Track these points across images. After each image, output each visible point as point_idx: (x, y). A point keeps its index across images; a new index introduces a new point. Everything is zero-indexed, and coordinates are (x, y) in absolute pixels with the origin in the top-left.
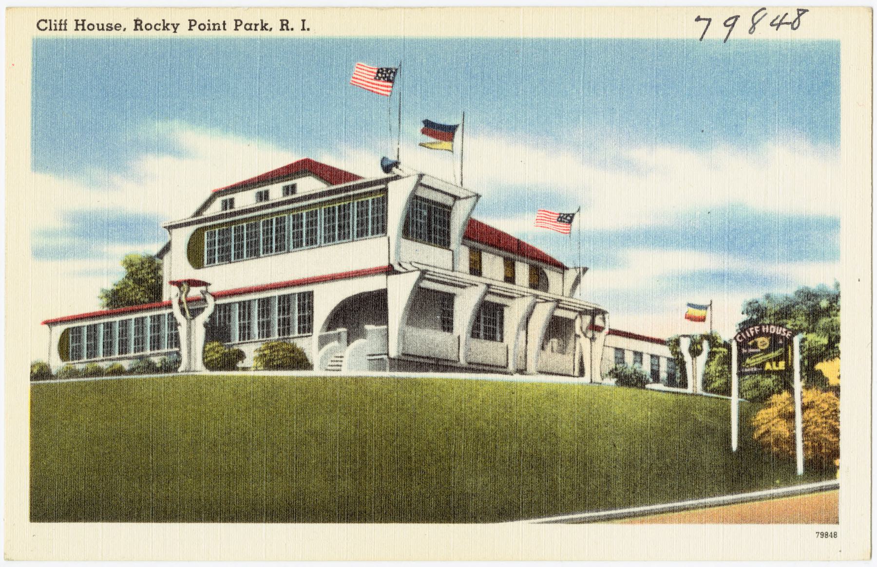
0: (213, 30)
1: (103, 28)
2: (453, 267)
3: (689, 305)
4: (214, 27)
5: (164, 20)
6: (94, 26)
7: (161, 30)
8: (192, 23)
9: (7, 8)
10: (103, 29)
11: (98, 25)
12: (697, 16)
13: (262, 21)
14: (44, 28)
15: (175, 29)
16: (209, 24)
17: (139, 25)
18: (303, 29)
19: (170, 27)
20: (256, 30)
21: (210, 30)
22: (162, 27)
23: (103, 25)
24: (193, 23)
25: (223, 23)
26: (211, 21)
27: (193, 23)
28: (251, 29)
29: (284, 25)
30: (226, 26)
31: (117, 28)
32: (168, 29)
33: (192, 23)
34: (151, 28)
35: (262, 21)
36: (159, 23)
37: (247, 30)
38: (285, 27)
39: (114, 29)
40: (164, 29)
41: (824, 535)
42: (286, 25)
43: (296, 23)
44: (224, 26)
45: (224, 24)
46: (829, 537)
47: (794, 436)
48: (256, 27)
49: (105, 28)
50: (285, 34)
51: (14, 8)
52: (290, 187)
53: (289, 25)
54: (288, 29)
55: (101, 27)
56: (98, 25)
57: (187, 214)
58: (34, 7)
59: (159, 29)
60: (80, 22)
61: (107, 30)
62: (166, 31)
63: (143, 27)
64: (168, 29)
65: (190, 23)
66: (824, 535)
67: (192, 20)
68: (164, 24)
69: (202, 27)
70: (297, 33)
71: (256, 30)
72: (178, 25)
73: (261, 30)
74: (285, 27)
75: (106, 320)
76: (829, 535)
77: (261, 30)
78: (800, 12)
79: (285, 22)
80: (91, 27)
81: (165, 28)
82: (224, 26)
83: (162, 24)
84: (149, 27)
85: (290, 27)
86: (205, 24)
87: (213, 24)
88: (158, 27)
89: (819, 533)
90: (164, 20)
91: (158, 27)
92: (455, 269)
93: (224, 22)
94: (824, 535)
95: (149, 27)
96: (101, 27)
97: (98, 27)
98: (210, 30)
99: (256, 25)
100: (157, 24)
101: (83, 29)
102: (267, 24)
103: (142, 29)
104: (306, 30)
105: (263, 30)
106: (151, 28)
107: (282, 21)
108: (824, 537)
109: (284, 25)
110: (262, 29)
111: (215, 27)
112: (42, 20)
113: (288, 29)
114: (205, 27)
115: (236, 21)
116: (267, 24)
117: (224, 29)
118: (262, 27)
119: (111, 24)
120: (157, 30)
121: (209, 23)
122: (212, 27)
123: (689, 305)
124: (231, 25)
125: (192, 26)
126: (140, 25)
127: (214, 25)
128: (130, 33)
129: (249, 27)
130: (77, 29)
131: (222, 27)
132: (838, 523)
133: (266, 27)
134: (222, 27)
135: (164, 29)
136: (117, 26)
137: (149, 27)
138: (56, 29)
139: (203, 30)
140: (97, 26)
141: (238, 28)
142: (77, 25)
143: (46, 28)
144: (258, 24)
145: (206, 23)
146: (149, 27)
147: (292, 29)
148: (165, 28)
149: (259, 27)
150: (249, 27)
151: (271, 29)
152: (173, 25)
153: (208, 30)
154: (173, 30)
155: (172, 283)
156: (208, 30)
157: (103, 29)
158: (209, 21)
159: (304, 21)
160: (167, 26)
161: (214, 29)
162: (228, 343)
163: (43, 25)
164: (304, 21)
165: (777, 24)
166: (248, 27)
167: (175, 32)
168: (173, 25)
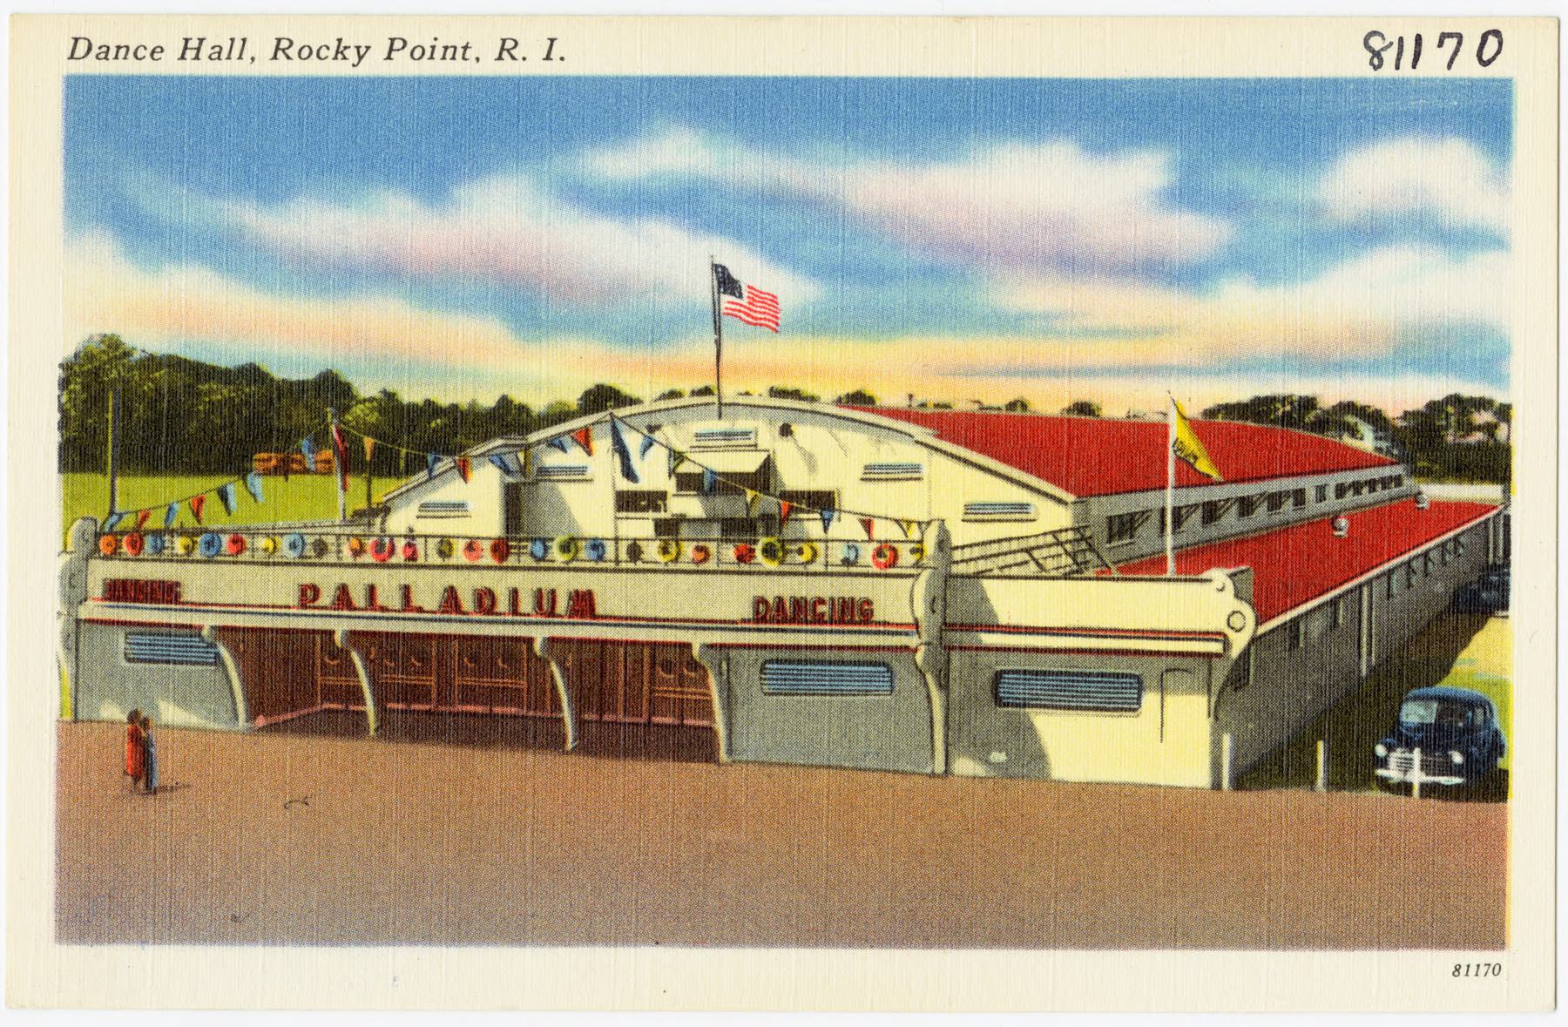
5: (340, 40)
15: (360, 58)
18: (548, 58)
22: (332, 53)
24: (398, 44)
29: (506, 49)
32: (345, 58)
34: (319, 51)
51: (969, 17)
52: (1487, 492)
60: (194, 43)
68: (339, 47)
75: (601, 565)
84: (305, 53)
90: (340, 40)
106: (319, 51)
117: (464, 58)
120: (141, 59)
121: (434, 43)
130: (183, 57)
140: (456, 56)
142: (186, 48)
148: (340, 52)
159: (552, 41)
164: (552, 41)
165: (217, 54)
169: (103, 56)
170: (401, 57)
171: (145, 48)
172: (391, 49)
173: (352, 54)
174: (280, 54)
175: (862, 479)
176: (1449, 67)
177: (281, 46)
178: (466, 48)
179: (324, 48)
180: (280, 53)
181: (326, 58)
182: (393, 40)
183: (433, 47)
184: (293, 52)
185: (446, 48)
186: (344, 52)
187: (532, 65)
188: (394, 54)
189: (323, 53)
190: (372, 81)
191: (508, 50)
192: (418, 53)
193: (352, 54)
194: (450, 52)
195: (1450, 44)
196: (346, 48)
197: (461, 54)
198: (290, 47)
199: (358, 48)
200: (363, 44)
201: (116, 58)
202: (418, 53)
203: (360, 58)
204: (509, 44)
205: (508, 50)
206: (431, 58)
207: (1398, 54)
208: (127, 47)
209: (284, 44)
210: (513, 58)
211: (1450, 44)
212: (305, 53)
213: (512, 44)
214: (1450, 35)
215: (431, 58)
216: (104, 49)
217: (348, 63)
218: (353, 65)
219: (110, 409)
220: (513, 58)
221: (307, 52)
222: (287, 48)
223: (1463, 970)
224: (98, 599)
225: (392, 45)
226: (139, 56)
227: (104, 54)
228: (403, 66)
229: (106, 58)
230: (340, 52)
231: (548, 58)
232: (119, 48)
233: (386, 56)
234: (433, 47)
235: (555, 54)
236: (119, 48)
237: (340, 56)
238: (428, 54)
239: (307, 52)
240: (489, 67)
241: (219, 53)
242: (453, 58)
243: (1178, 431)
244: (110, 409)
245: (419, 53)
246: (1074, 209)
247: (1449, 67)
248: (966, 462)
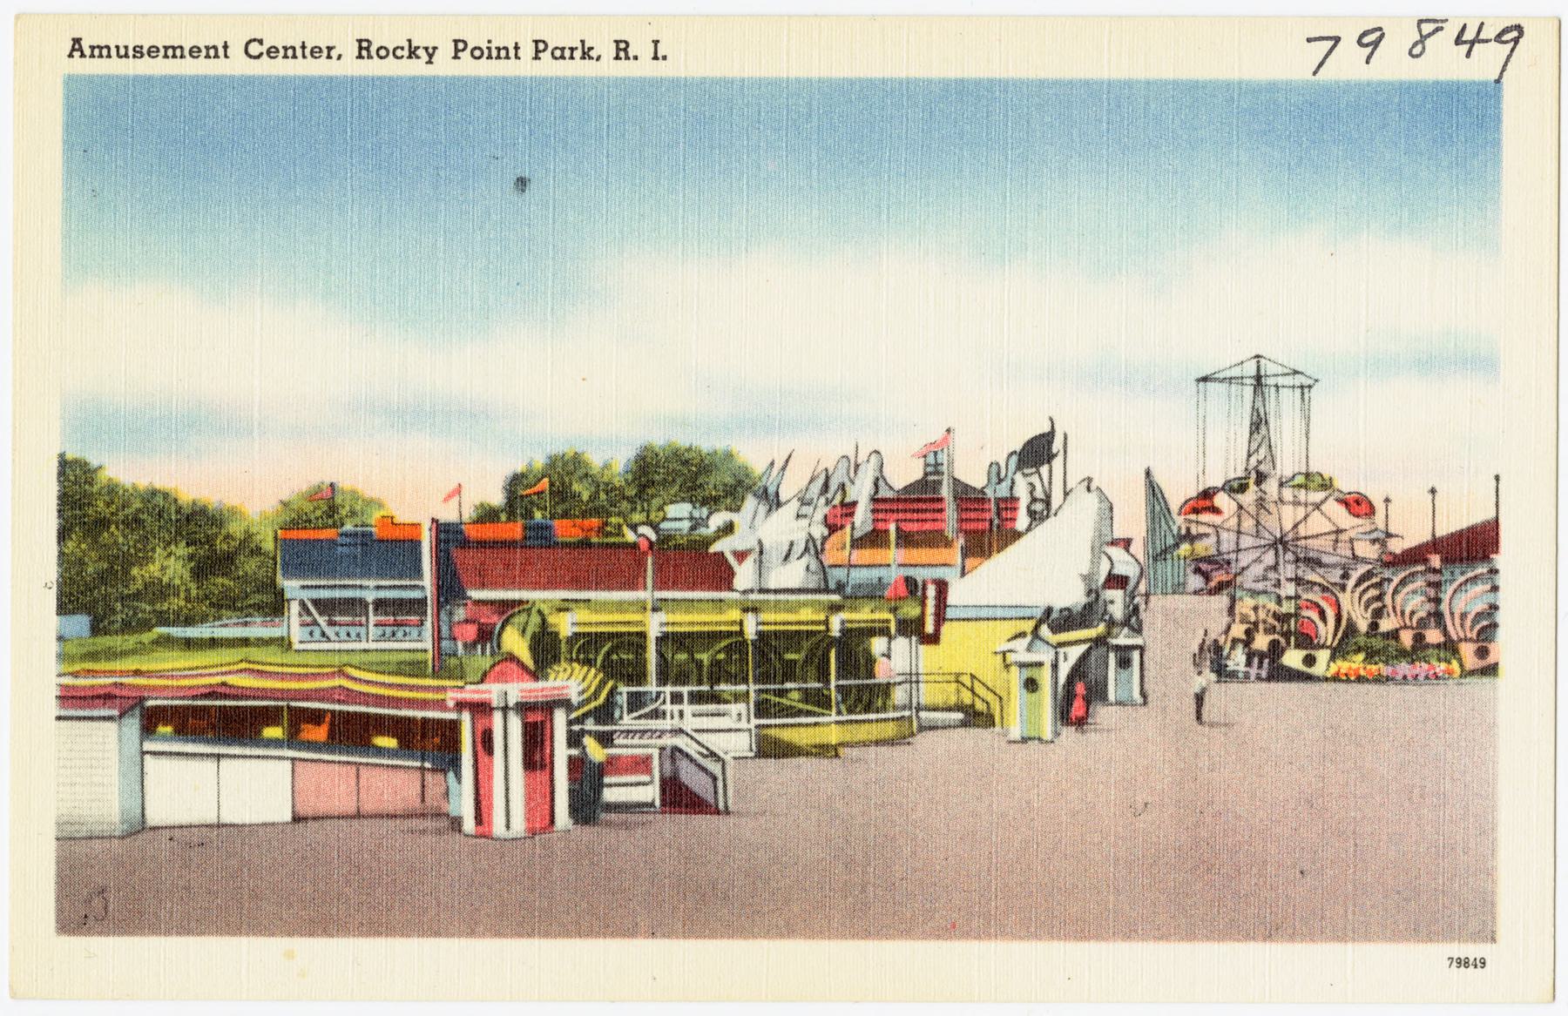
0: (98, 57)
1: (174, 51)
4: (92, 52)
5: (410, 41)
6: (378, 54)
7: (405, 58)
8: (459, 46)
9: (17, 17)
10: (126, 56)
11: (117, 47)
12: (79, 37)
13: (583, 42)
14: (257, 54)
15: (431, 56)
16: (489, 49)
17: (365, 48)
18: (656, 58)
19: (421, 52)
20: (572, 58)
21: (492, 58)
22: (406, 53)
23: (126, 47)
24: (461, 46)
25: (514, 45)
26: (493, 41)
27: (461, 46)
28: (562, 57)
29: (622, 49)
30: (228, 50)
31: (315, 55)
32: (418, 57)
33: (459, 46)
34: (388, 55)
35: (583, 42)
36: (401, 45)
37: (556, 58)
38: (622, 54)
39: (146, 56)
40: (410, 57)
41: (1463, 963)
42: (625, 50)
43: (642, 47)
44: (226, 51)
45: (517, 48)
46: (1472, 967)
47: (377, 610)
48: (572, 54)
49: (131, 53)
50: (624, 69)
53: (629, 50)
54: (627, 58)
55: (122, 52)
56: (117, 47)
57: (1346, 490)
58: (758, 16)
59: (402, 57)
61: (134, 56)
62: (414, 60)
63: (373, 52)
64: (418, 57)
65: (456, 46)
66: (1463, 962)
67: (540, 41)
68: (410, 46)
69: (477, 53)
70: (644, 68)
71: (572, 58)
72: (435, 48)
73: (581, 58)
74: (622, 54)
76: (1470, 963)
77: (581, 58)
78: (1427, 28)
79: (365, 44)
80: (383, 53)
81: (586, 56)
82: (226, 51)
83: (407, 48)
85: (631, 55)
86: (481, 46)
87: (496, 48)
88: (399, 53)
89: (1452, 959)
90: (410, 41)
91: (399, 53)
93: (516, 44)
94: (1463, 963)
95: (383, 53)
96: (122, 52)
97: (182, 51)
98: (492, 58)
99: (572, 49)
100: (398, 48)
101: (370, 57)
102: (592, 48)
103: (370, 57)
104: (632, 58)
105: (585, 58)
107: (360, 41)
108: (1463, 967)
109: (622, 49)
110: (583, 58)
111: (502, 53)
112: (255, 40)
113: (627, 58)
114: (483, 53)
115: (456, 42)
116: (592, 48)
117: (226, 56)
118: (584, 53)
119: (141, 47)
122: (494, 53)
124: (527, 50)
125: (540, 51)
126: (368, 49)
127: (499, 49)
128: (350, 66)
129: (560, 54)
131: (221, 52)
132: (1494, 940)
134: (221, 52)
135: (410, 57)
136: (152, 49)
137: (383, 53)
138: (490, 57)
139: (479, 58)
141: (541, 55)
143: (261, 54)
144: (576, 48)
145: (484, 46)
146: (383, 53)
147: (636, 58)
148: (413, 53)
149: (577, 54)
150: (560, 54)
151: (598, 59)
152: (426, 49)
153: (487, 58)
154: (427, 59)
156: (487, 58)
157: (126, 56)
158: (489, 42)
159: (656, 42)
160: (415, 51)
161: (498, 57)
162: (868, 682)
163: (255, 49)
164: (656, 42)
166: (558, 53)
167: (430, 62)
168: (426, 49)
172: (537, 51)
175: (59, 718)
176: (1315, 73)
178: (330, 49)
181: (402, 57)
190: (1347, 87)
197: (223, 53)
200: (431, 45)
219: (750, 648)
228: (467, 67)
244: (750, 648)
246: (1379, 360)
247: (1315, 73)
248: (91, 719)
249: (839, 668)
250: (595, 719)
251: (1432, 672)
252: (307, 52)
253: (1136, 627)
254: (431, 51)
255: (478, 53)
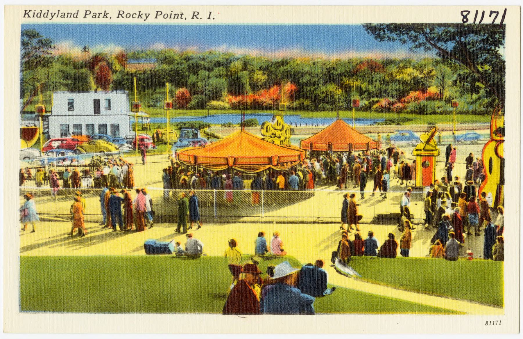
2: (451, 130)
3: (484, 12)
5: (140, 12)
7: (136, 18)
15: (147, 18)
18: (209, 18)
22: (137, 16)
24: (159, 13)
29: (195, 15)
32: (141, 18)
40: (138, 18)
62: (140, 19)
64: (141, 18)
84: (128, 16)
90: (140, 12)
92: (452, 129)
111: (70, 15)
117: (181, 18)
118: (139, 15)
121: (171, 13)
123: (484, 12)
133: (107, 15)
148: (140, 16)
149: (102, 16)
155: (353, 229)
159: (210, 13)
164: (210, 13)
169: (63, 16)
170: (160, 18)
171: (136, 14)
172: (157, 15)
173: (144, 16)
174: (195, 17)
177: (120, 13)
178: (182, 14)
179: (135, 14)
180: (194, 17)
182: (86, 11)
183: (171, 14)
184: (124, 15)
185: (175, 15)
186: (29, 13)
187: (203, 21)
188: (158, 17)
189: (134, 16)
191: (121, 15)
192: (166, 16)
193: (144, 16)
194: (177, 16)
195: (494, 15)
196: (142, 14)
198: (123, 14)
199: (146, 14)
200: (148, 13)
201: (67, 17)
202: (166, 16)
203: (52, 17)
204: (196, 14)
205: (121, 15)
206: (170, 18)
207: (502, 19)
208: (71, 14)
209: (121, 13)
210: (197, 18)
211: (494, 15)
212: (128, 16)
213: (122, 12)
214: (495, 12)
215: (170, 18)
216: (95, 14)
217: (143, 20)
218: (144, 20)
220: (197, 18)
221: (128, 16)
222: (198, 15)
223: (489, 323)
224: (251, 78)
225: (194, 13)
226: (134, 17)
227: (63, 16)
228: (161, 20)
229: (95, 17)
230: (140, 16)
231: (209, 18)
232: (99, 14)
233: (155, 17)
234: (171, 14)
235: (211, 17)
236: (68, 14)
237: (140, 17)
238: (169, 16)
239: (128, 16)
240: (191, 22)
241: (96, 15)
242: (178, 18)
243: (93, 85)
245: (166, 16)
249: (483, 165)
250: (496, 45)
251: (348, 98)
252: (60, 15)
253: (468, 13)
254: (53, 14)
255: (166, 16)
